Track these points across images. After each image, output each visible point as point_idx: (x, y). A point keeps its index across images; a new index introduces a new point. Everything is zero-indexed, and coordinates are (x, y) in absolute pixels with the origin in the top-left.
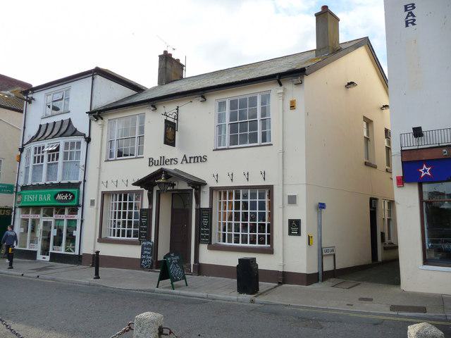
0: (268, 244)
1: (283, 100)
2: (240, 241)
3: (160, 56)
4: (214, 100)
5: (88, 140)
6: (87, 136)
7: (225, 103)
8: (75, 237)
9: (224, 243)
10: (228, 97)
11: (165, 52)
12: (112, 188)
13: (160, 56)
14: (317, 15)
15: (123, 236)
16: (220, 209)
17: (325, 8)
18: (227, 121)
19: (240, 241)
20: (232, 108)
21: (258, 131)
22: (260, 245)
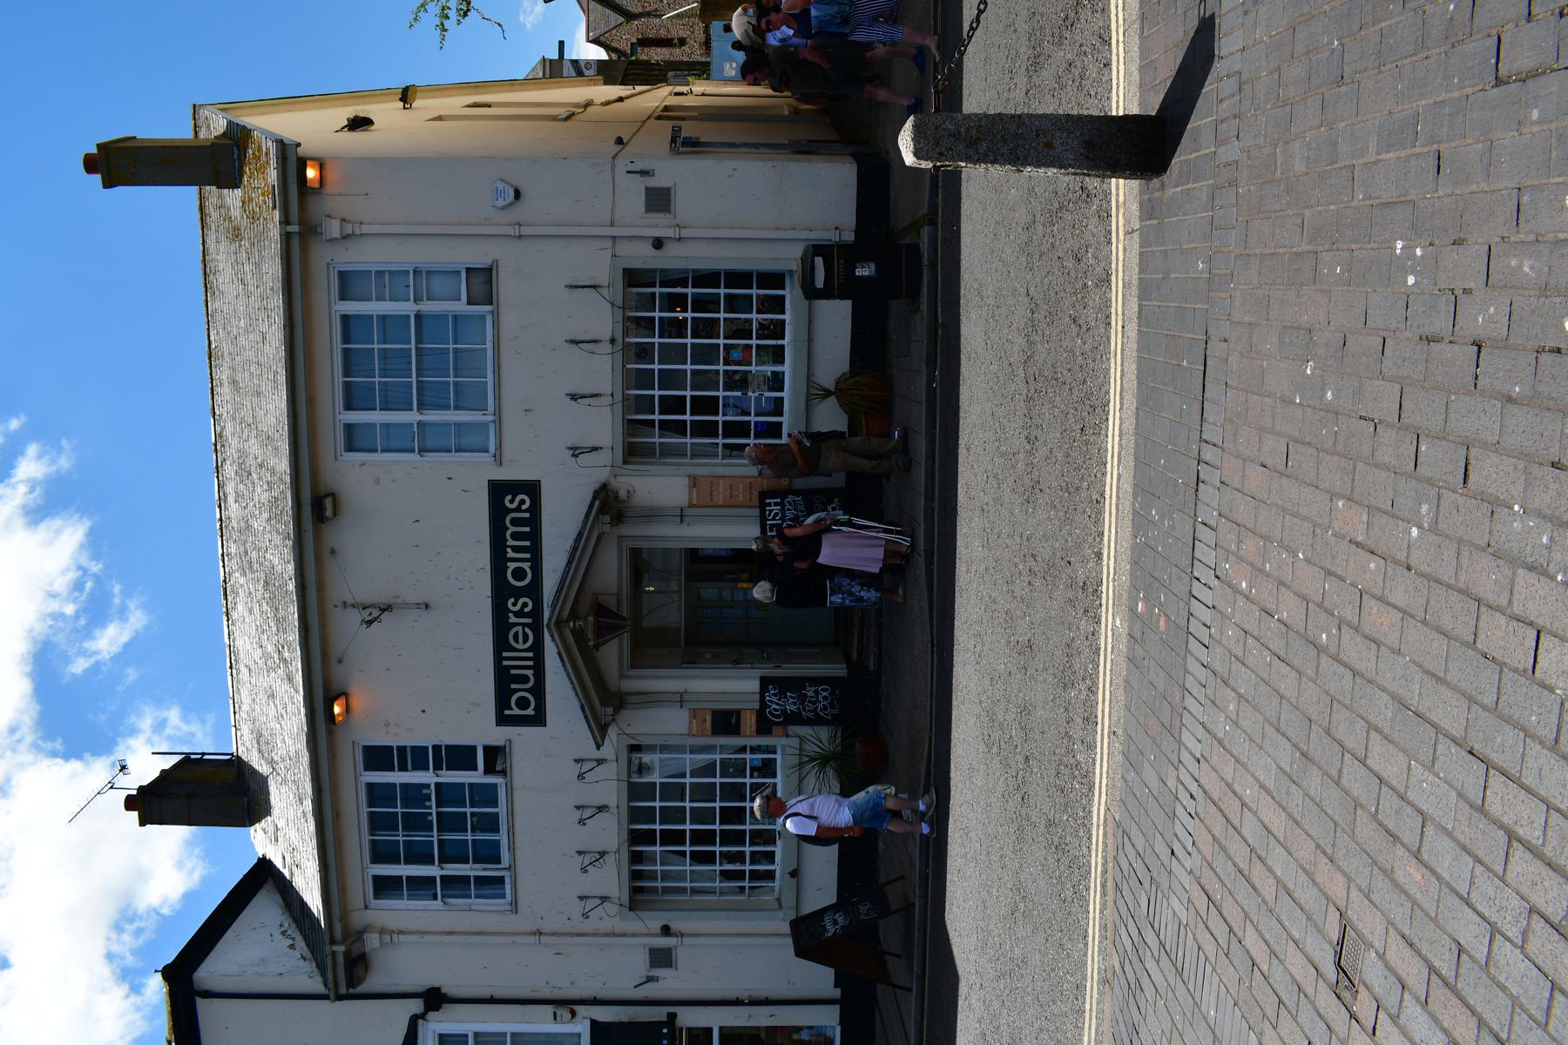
0: (774, 843)
1: (400, 932)
2: (780, 342)
3: (143, 822)
4: (353, 474)
5: (434, 999)
6: (416, 1006)
7: (349, 428)
8: (805, 59)
9: (778, 858)
10: (335, 416)
11: (130, 803)
12: (611, 879)
13: (143, 822)
14: (109, 183)
15: (770, 857)
16: (683, 890)
17: (91, 164)
18: (427, 777)
19: (780, 342)
20: (394, 859)
21: (472, 874)
22: (788, 312)
